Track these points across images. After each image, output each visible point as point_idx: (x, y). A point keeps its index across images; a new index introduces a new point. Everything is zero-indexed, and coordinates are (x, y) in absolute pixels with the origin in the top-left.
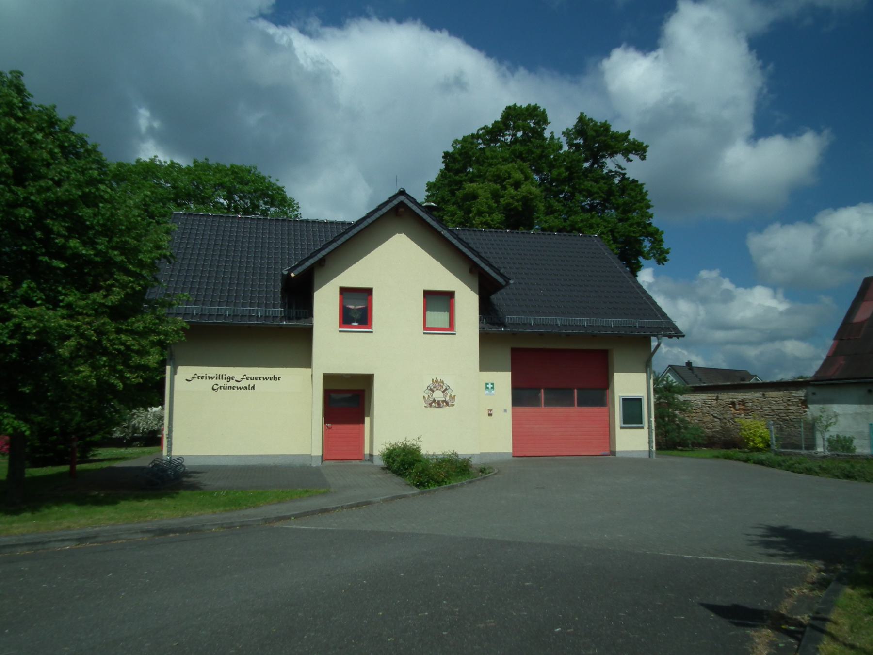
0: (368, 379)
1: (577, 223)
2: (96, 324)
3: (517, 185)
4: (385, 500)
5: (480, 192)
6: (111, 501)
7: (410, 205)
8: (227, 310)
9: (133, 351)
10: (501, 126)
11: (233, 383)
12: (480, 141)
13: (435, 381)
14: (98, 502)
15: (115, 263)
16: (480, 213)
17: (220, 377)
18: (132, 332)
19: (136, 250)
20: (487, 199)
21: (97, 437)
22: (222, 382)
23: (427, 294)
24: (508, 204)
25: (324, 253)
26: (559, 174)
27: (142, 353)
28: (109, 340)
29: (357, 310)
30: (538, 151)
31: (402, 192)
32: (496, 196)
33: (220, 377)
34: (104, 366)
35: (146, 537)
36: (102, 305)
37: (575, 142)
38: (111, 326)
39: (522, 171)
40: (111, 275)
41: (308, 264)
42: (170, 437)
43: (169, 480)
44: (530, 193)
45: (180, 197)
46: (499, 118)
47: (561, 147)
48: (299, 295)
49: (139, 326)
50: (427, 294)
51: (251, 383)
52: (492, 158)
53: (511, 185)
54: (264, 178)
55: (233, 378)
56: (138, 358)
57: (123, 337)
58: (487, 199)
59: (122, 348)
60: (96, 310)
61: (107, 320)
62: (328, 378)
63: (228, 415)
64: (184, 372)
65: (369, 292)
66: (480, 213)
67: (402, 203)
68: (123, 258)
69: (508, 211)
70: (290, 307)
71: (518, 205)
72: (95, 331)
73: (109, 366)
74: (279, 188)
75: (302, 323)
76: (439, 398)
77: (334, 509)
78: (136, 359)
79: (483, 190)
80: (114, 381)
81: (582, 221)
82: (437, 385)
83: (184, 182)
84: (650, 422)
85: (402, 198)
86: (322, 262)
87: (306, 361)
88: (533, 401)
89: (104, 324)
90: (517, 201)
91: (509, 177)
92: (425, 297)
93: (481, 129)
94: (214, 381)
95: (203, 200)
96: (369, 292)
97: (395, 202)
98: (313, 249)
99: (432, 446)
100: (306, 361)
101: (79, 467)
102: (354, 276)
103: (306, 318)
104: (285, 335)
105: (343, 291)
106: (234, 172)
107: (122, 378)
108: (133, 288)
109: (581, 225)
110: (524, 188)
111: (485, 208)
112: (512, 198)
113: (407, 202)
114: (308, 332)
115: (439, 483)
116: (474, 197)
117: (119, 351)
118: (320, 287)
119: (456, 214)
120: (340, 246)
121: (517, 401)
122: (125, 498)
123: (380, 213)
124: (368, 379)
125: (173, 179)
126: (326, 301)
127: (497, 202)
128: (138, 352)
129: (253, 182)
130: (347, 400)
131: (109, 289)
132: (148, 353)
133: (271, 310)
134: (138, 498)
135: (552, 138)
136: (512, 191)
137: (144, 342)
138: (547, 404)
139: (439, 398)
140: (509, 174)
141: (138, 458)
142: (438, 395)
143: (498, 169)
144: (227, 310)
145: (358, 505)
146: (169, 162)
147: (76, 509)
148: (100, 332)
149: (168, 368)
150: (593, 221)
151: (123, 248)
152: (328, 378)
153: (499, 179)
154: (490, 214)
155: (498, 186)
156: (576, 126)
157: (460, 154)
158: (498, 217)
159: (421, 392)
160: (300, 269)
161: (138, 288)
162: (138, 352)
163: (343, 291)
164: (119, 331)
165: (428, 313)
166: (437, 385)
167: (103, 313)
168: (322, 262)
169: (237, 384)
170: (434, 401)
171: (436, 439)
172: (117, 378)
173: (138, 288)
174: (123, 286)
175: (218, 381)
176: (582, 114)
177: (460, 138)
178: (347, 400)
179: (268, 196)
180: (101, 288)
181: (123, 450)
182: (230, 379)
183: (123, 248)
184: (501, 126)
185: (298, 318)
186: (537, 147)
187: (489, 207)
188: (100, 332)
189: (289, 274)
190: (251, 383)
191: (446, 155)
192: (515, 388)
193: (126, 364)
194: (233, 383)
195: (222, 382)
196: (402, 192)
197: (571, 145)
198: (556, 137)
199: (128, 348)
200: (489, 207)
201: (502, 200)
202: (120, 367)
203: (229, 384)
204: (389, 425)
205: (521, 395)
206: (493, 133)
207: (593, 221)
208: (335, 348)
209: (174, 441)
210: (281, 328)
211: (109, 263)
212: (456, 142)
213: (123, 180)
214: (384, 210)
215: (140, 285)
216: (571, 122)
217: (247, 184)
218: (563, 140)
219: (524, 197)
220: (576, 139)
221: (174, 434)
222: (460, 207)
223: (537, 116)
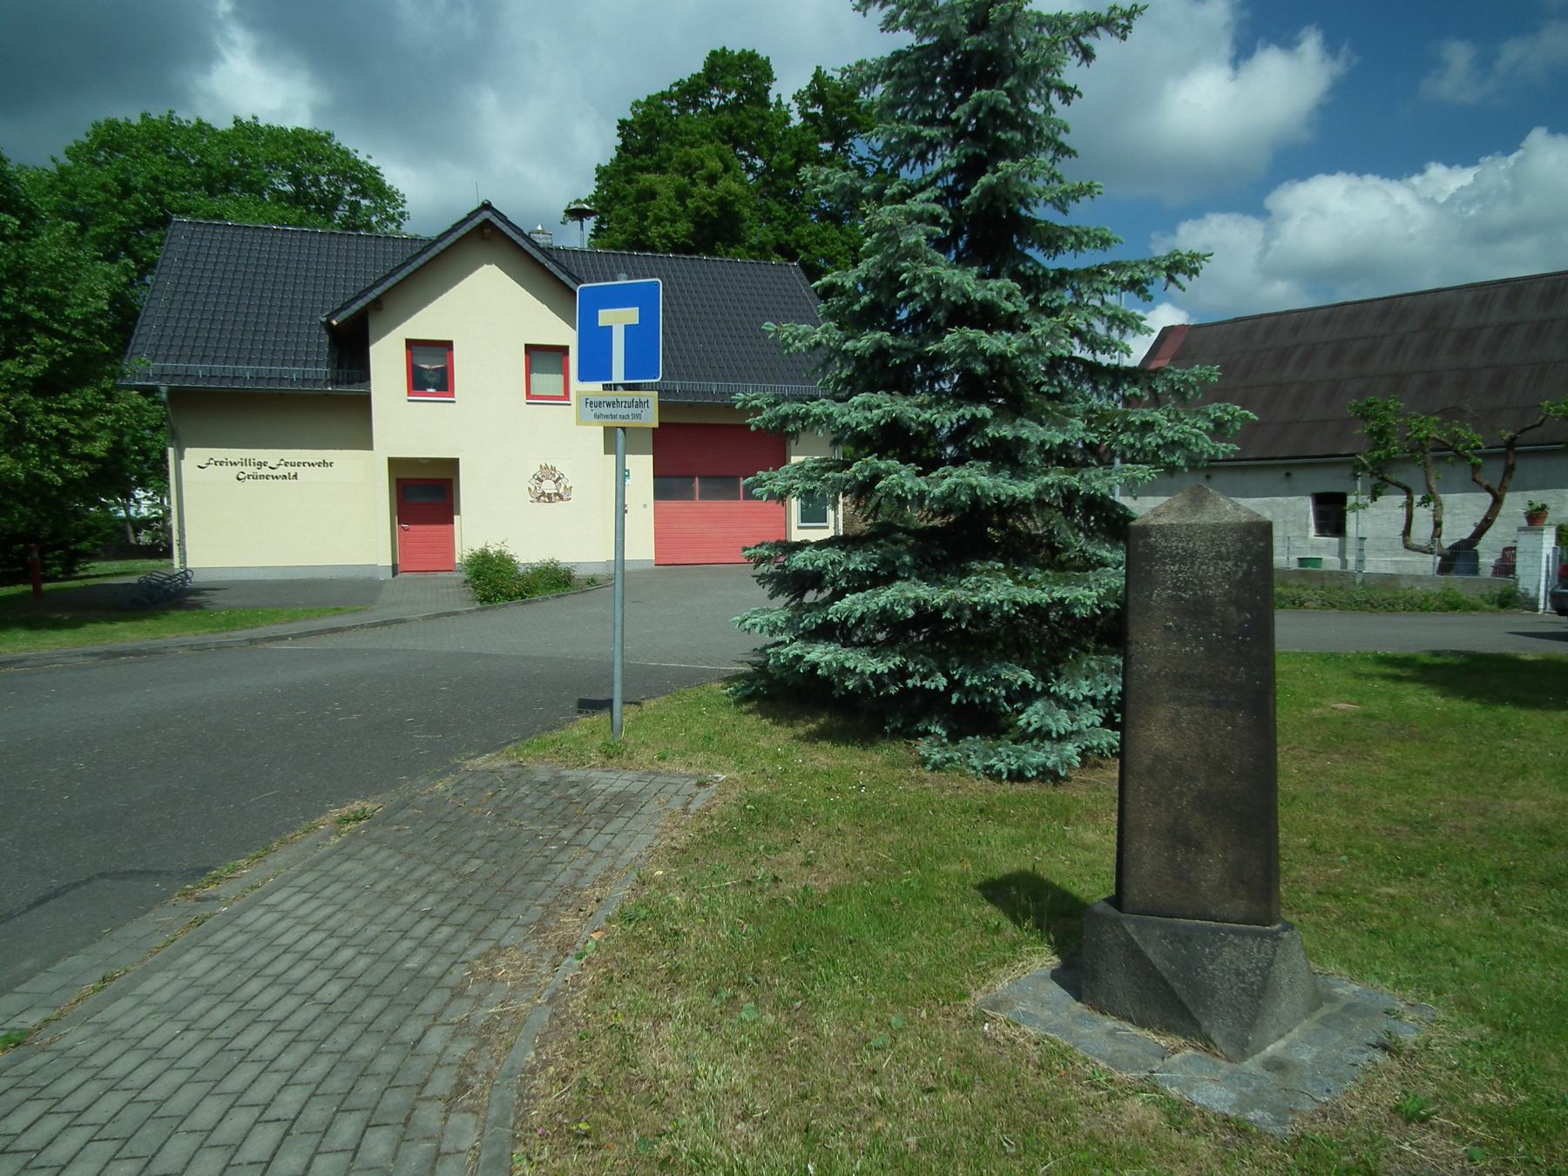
0: (453, 464)
1: (802, 237)
2: (13, 402)
3: (712, 180)
4: (424, 618)
5: (659, 188)
6: (74, 624)
7: (500, 224)
8: (247, 370)
9: (73, 436)
10: (703, 82)
11: (265, 471)
12: (675, 103)
13: (544, 468)
14: (56, 625)
15: (35, 321)
16: (658, 221)
17: (245, 462)
18: (68, 412)
19: (63, 303)
20: (669, 199)
21: (85, 545)
22: (250, 470)
23: (530, 349)
24: (698, 209)
25: (377, 292)
26: (782, 162)
27: (86, 438)
28: (33, 422)
29: (432, 371)
30: (754, 125)
31: (487, 206)
32: (682, 195)
33: (245, 462)
34: (34, 456)
35: (90, 660)
36: (21, 376)
37: (811, 110)
38: (37, 405)
39: (722, 159)
40: (29, 338)
41: (356, 307)
42: (182, 543)
43: (172, 597)
44: (729, 193)
45: (219, 182)
46: (699, 68)
47: (787, 120)
48: (350, 347)
49: (77, 404)
50: (530, 349)
51: (293, 470)
52: (687, 134)
53: (704, 179)
54: (346, 153)
55: (265, 464)
56: (78, 444)
57: (54, 418)
58: (669, 199)
59: (54, 433)
60: (12, 384)
61: (27, 396)
62: (394, 464)
63: (257, 514)
64: (194, 456)
65: (448, 345)
66: (658, 221)
67: (487, 222)
68: (42, 314)
69: (699, 219)
70: (340, 366)
71: (712, 210)
72: (13, 411)
73: (41, 456)
74: (371, 169)
75: (355, 389)
76: (549, 489)
77: (349, 628)
78: (76, 447)
79: (664, 184)
80: (47, 474)
81: (810, 234)
82: (547, 472)
83: (216, 157)
84: (836, 520)
85: (487, 214)
86: (377, 304)
87: (365, 442)
88: (686, 494)
89: (25, 401)
90: (711, 204)
91: (702, 167)
92: (526, 352)
93: (677, 84)
94: (239, 468)
95: (254, 188)
96: (448, 345)
97: (478, 220)
98: (361, 286)
99: (528, 553)
100: (365, 442)
101: (46, 586)
102: (425, 323)
103: (361, 381)
104: (331, 403)
105: (411, 344)
106: (298, 142)
107: (59, 470)
108: (63, 355)
109: (807, 240)
110: (721, 185)
111: (665, 213)
112: (704, 199)
113: (494, 220)
114: (366, 400)
115: (510, 597)
116: (650, 194)
117: (50, 435)
118: (379, 338)
119: (627, 220)
120: (400, 282)
121: (660, 493)
122: (95, 621)
123: (456, 236)
124: (453, 464)
125: (198, 152)
126: (387, 358)
127: (683, 204)
128: (79, 437)
129: (328, 158)
130: (425, 492)
131: (27, 355)
132: (94, 439)
133: (317, 371)
134: (110, 620)
135: (779, 103)
136: (703, 188)
137: (86, 424)
138: (703, 496)
139: (549, 489)
140: (702, 162)
141: (134, 571)
142: (549, 486)
143: (686, 154)
144: (247, 370)
145: (385, 623)
146: (194, 122)
147: (22, 634)
148: (20, 413)
149: (171, 451)
150: (826, 235)
151: (43, 301)
152: (394, 464)
153: (688, 169)
154: (673, 222)
155: (686, 180)
156: (810, 87)
157: (642, 125)
158: (684, 227)
159: (527, 481)
160: (344, 315)
161: (69, 354)
162: (79, 437)
163: (411, 344)
164: (48, 411)
165: (534, 376)
166: (547, 472)
167: (23, 387)
168: (377, 304)
169: (274, 473)
170: (543, 494)
171: (531, 541)
172: (54, 471)
173: (69, 354)
174: (49, 352)
175: (243, 469)
176: (818, 68)
177: (643, 99)
178: (425, 492)
179: (359, 181)
180: (17, 354)
181: (152, 562)
182: (261, 464)
183: (43, 301)
184: (703, 82)
185: (350, 382)
186: (754, 119)
187: (672, 211)
188: (20, 413)
189: (329, 322)
190: (293, 470)
191: (623, 125)
192: (657, 475)
193: (64, 451)
194: (265, 471)
195: (250, 470)
196: (487, 206)
197: (804, 114)
198: (784, 102)
199: (65, 432)
200: (672, 211)
201: (689, 202)
202: (55, 457)
203: (260, 472)
204: (484, 523)
205: (667, 484)
206: (690, 92)
207: (826, 235)
208: (403, 424)
209: (188, 549)
210: (327, 395)
211: (25, 320)
212: (637, 104)
213: (119, 148)
214: (462, 231)
215: (71, 349)
216: (803, 82)
217: (319, 162)
218: (795, 106)
219: (721, 199)
220: (812, 106)
221: (188, 540)
222: (634, 211)
223: (757, 67)
